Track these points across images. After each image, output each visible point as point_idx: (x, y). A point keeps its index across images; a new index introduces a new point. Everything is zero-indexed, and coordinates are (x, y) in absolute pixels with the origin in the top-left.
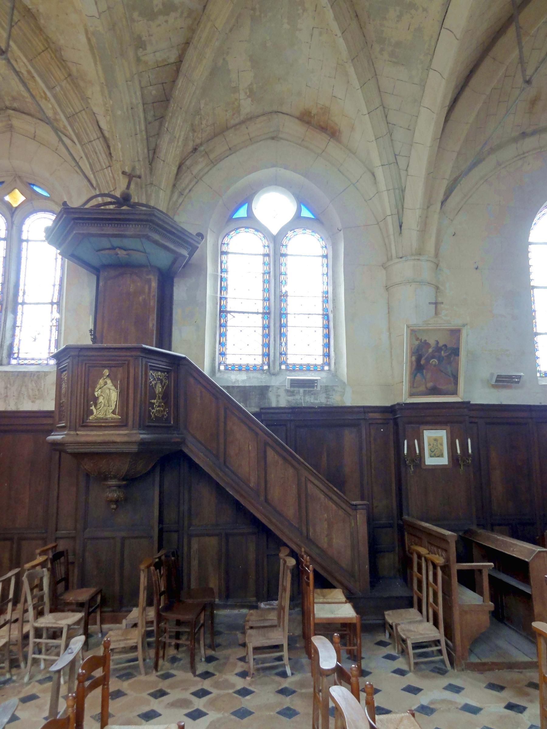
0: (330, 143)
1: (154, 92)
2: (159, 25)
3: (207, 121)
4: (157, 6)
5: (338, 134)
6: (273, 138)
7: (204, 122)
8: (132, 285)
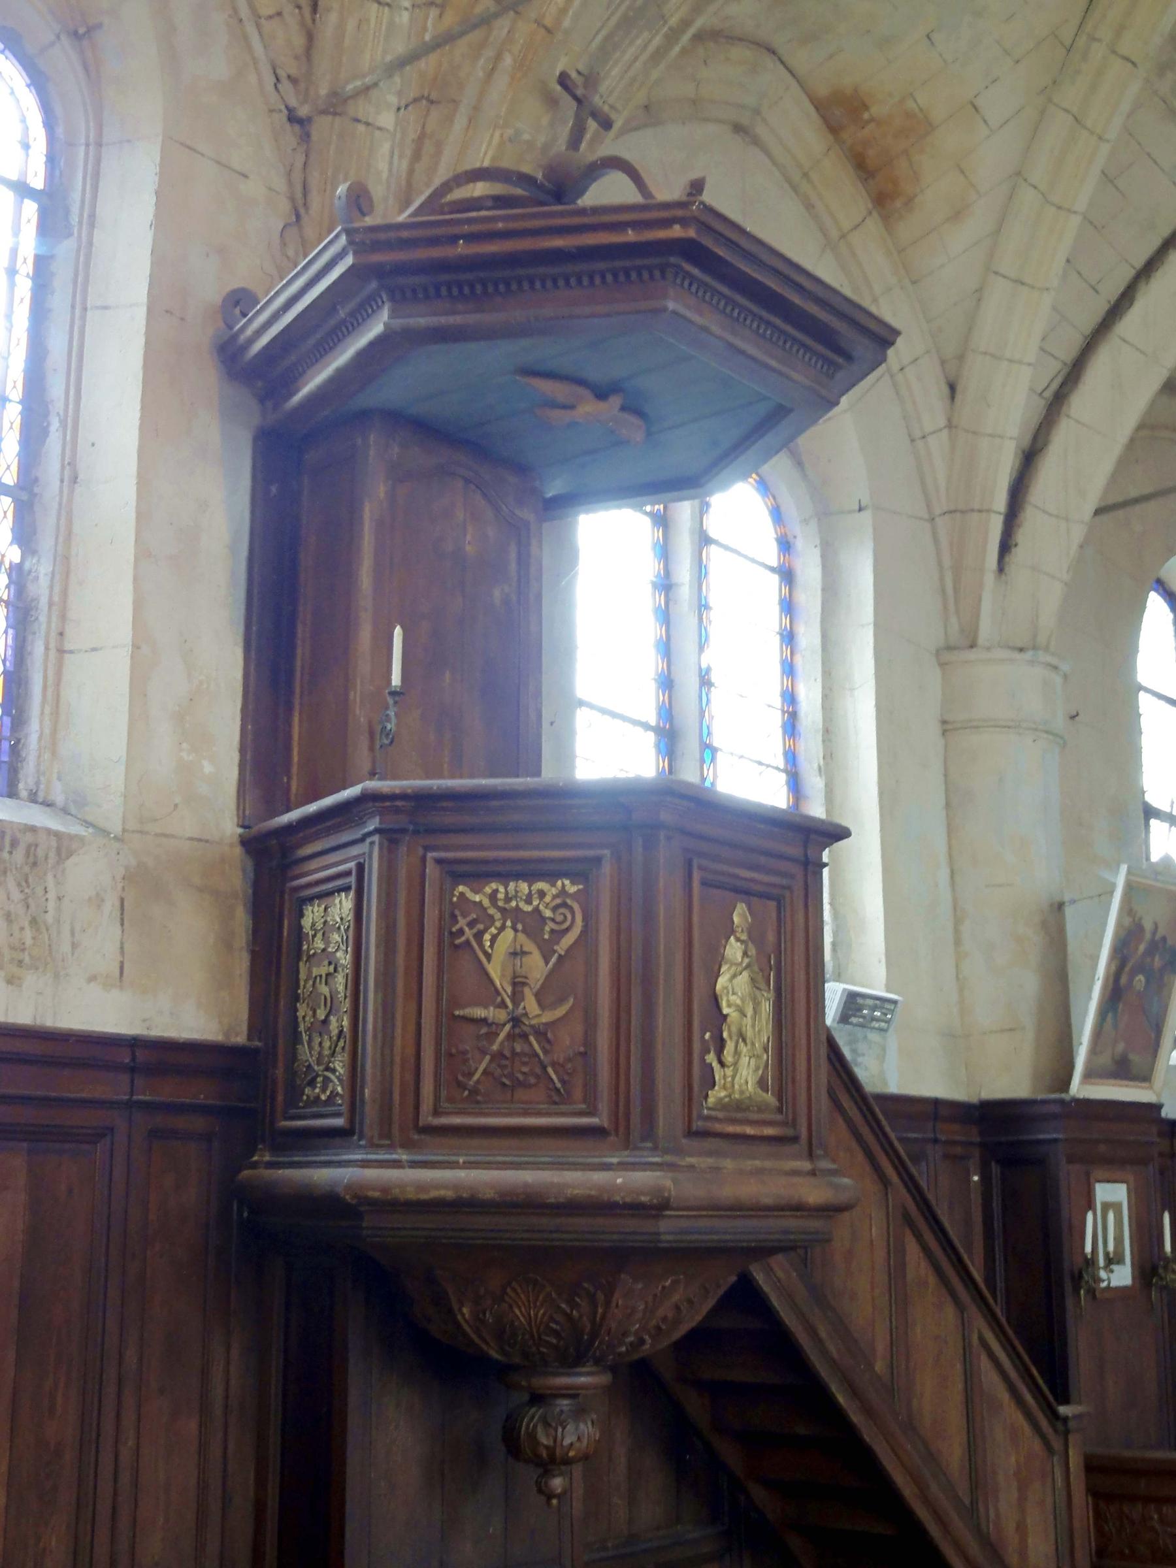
0: (869, 222)
5: (898, 204)
6: (738, 128)
8: (470, 529)
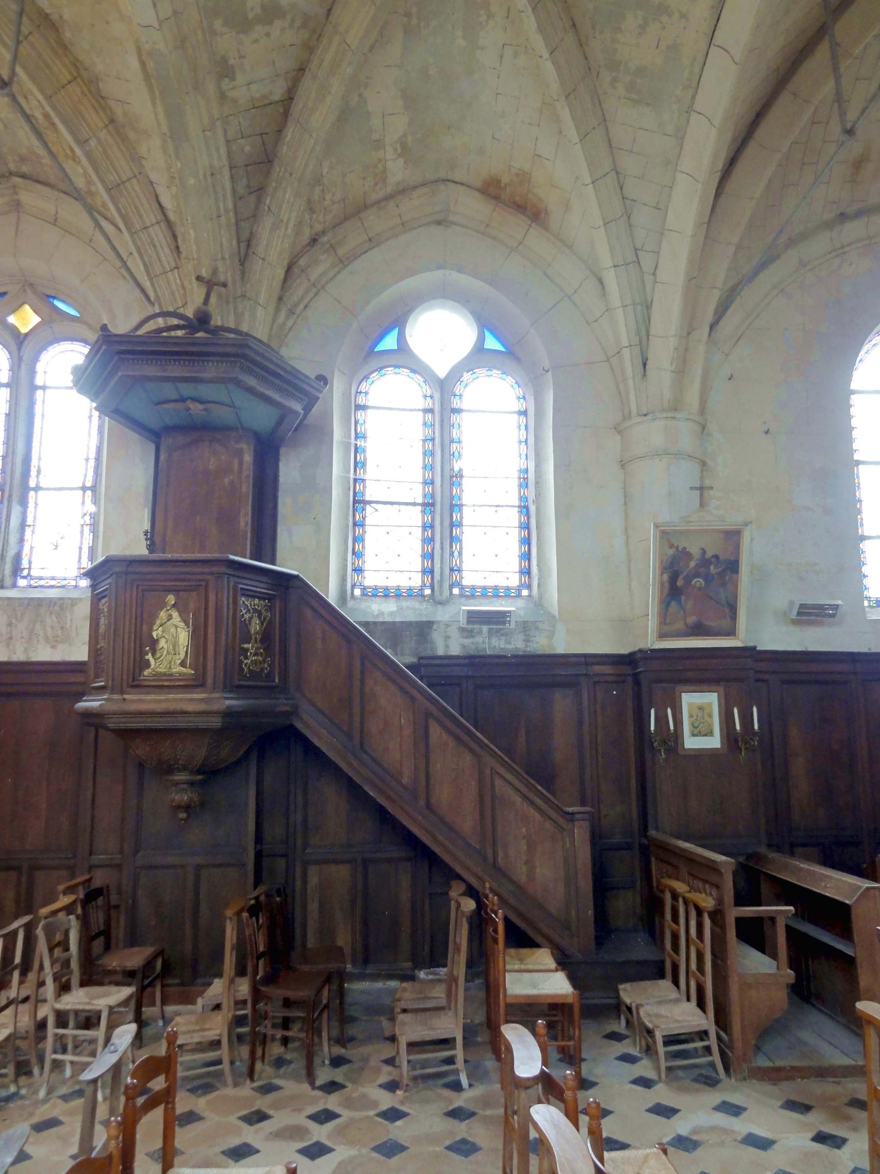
0: (531, 230)
1: (248, 149)
2: (257, 41)
3: (333, 195)
4: (252, 9)
5: (543, 215)
6: (439, 223)
7: (328, 197)
8: (212, 459)
